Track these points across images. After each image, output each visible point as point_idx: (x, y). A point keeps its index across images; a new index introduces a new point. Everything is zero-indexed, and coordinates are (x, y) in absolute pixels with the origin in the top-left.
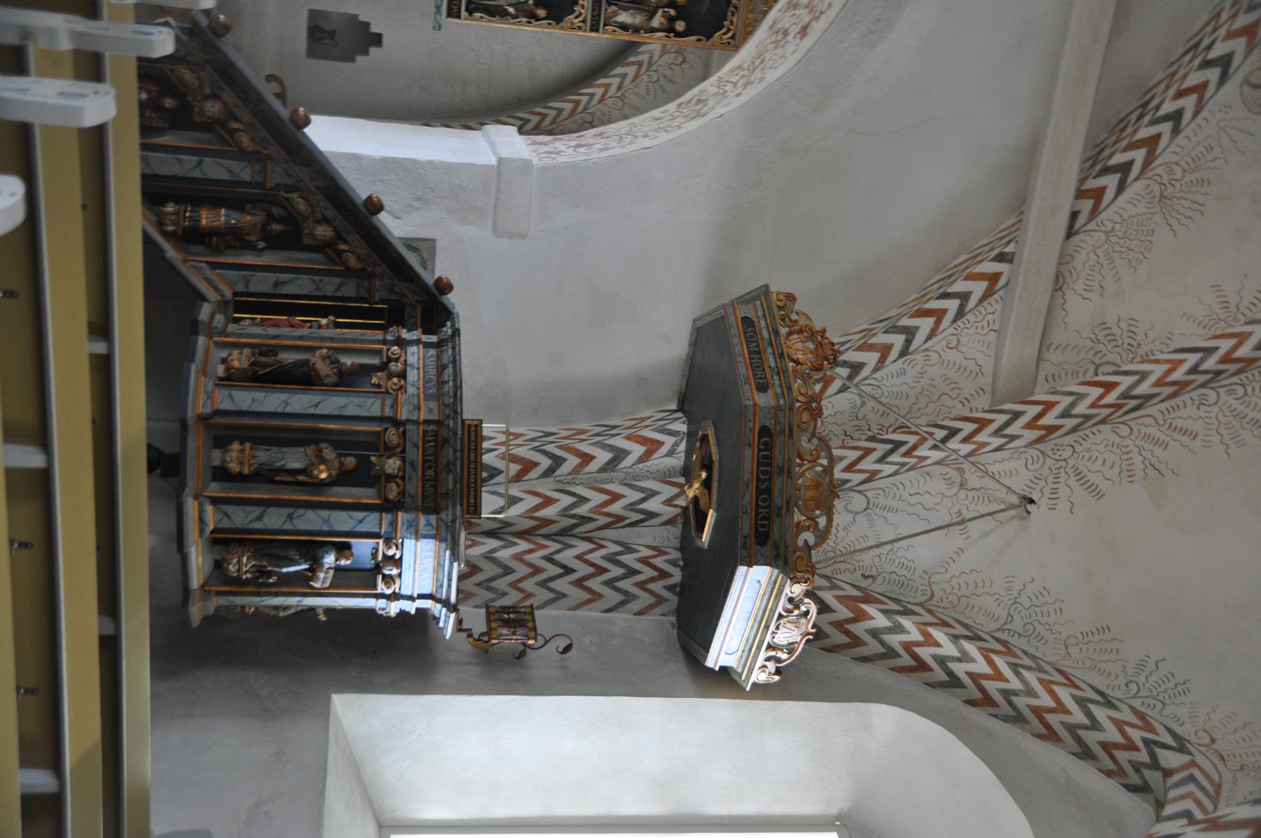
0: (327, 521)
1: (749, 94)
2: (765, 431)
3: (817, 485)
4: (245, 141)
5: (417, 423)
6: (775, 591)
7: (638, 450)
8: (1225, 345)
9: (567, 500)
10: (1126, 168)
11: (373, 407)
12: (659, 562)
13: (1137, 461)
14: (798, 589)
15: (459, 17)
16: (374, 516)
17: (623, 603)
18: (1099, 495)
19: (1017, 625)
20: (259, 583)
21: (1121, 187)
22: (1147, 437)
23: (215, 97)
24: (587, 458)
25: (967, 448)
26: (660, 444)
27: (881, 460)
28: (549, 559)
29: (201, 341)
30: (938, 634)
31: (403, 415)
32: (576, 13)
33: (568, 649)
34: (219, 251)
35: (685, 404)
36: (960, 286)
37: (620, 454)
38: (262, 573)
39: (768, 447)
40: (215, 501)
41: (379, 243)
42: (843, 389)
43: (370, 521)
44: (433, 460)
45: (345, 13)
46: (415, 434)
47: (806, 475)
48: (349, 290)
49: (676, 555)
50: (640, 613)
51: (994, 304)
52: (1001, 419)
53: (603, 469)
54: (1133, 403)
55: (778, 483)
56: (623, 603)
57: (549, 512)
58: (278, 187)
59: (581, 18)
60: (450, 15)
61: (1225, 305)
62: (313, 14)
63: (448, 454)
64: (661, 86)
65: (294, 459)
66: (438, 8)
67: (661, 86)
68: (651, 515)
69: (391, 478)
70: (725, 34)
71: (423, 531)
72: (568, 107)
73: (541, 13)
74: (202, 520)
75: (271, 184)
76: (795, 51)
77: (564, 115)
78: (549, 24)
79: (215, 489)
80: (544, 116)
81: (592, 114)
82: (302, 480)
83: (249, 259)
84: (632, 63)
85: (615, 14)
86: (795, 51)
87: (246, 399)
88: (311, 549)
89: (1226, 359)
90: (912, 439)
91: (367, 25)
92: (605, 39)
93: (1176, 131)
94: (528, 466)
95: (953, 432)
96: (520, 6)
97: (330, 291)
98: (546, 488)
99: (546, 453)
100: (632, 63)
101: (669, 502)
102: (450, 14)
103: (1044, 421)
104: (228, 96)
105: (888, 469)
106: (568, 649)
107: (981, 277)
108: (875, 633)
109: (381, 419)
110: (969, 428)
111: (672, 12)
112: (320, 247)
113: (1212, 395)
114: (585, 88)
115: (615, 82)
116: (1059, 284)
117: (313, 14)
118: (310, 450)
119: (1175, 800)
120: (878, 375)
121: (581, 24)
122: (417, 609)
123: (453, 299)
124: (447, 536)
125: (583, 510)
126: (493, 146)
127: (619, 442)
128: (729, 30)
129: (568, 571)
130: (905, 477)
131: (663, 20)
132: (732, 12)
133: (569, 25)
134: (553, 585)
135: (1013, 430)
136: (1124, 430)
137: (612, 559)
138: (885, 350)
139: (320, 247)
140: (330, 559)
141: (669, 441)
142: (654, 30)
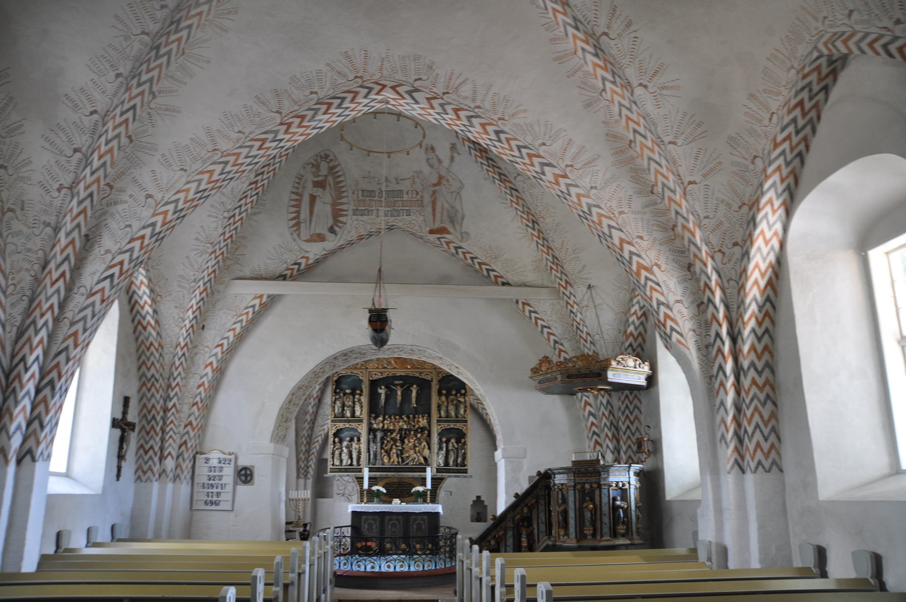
0: (605, 504)
1: (476, 382)
2: (568, 377)
3: (582, 360)
4: (501, 533)
5: (575, 480)
6: (615, 369)
7: (588, 408)
8: (535, 239)
9: (606, 429)
10: (488, 270)
11: (571, 493)
12: (623, 398)
13: (573, 256)
14: (614, 363)
16: (603, 490)
17: (638, 409)
18: (584, 266)
19: (626, 287)
20: (627, 523)
21: (493, 270)
22: (566, 254)
23: (489, 542)
24: (593, 424)
25: (576, 306)
26: (586, 401)
27: (582, 332)
28: (625, 433)
29: (558, 543)
30: (633, 311)
31: (572, 484)
33: (649, 427)
34: (534, 540)
35: (573, 394)
36: (527, 313)
37: (590, 413)
38: (623, 523)
39: (572, 375)
40: (602, 536)
41: (528, 493)
42: (562, 344)
43: (604, 491)
44: (586, 473)
46: (578, 480)
47: (580, 364)
48: (542, 502)
49: (620, 393)
50: (640, 402)
51: (531, 303)
52: (565, 298)
53: (595, 418)
54: (556, 260)
55: (583, 371)
56: (638, 409)
57: (610, 435)
58: (514, 524)
60: (466, 473)
61: (525, 236)
62: (472, 521)
63: (583, 470)
65: (588, 515)
66: (465, 477)
68: (608, 402)
69: (591, 486)
71: (606, 476)
73: (463, 441)
74: (607, 540)
75: (512, 525)
76: (462, 370)
79: (598, 537)
82: (594, 512)
83: (536, 532)
86: (462, 370)
87: (572, 530)
88: (615, 508)
89: (539, 238)
90: (575, 323)
92: (470, 417)
93: (476, 258)
94: (597, 442)
95: (571, 311)
97: (543, 507)
98: (603, 436)
99: (592, 437)
101: (603, 397)
102: (466, 472)
103: (564, 285)
104: (489, 538)
105: (585, 329)
106: (649, 427)
107: (523, 308)
108: (636, 329)
109: (575, 490)
110: (569, 307)
112: (530, 511)
113: (551, 239)
116: (525, 285)
117: (472, 521)
118: (585, 510)
119: (838, 50)
120: (557, 335)
122: (390, 503)
123: (542, 471)
124: (606, 468)
125: (608, 424)
126: (500, 460)
127: (586, 413)
129: (628, 427)
130: (587, 323)
134: (633, 431)
135: (568, 294)
136: (564, 261)
137: (623, 413)
138: (549, 333)
139: (530, 511)
140: (618, 503)
141: (585, 398)
142: (465, 401)
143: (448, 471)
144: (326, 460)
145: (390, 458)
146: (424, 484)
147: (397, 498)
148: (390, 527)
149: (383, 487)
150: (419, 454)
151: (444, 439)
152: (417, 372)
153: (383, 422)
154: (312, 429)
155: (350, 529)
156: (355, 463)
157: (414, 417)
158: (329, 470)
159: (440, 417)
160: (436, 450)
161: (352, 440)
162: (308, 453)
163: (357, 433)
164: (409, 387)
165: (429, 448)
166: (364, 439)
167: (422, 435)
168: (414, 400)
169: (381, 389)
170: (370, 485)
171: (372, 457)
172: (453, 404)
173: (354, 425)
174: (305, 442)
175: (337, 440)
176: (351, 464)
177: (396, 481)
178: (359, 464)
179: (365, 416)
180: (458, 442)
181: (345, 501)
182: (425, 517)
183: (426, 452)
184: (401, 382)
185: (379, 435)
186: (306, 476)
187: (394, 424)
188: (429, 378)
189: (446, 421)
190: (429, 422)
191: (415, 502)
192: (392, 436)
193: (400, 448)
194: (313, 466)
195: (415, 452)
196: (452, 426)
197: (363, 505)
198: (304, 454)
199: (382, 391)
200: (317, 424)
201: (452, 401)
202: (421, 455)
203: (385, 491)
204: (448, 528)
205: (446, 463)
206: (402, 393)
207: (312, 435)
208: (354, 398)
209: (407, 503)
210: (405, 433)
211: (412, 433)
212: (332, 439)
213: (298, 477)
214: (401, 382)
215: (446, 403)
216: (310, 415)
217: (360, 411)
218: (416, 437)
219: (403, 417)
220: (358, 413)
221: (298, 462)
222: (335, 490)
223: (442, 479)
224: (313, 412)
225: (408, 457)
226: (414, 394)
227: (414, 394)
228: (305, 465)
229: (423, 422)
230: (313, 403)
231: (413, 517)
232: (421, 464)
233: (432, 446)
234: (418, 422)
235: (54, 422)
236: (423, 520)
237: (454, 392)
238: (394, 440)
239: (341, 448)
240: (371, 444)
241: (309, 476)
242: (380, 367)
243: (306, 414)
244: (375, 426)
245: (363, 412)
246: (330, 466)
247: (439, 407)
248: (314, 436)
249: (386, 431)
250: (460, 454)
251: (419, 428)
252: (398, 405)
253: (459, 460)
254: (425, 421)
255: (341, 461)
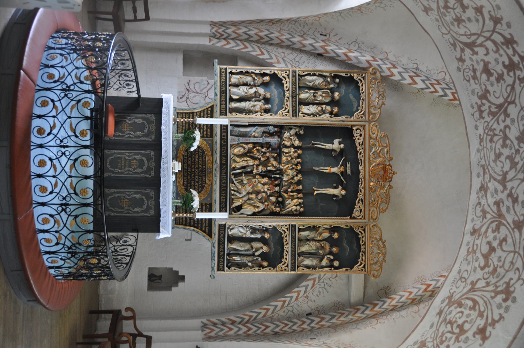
15: (223, 270)
32: (283, 262)
45: (166, 268)
59: (286, 265)
60: (219, 270)
62: (150, 269)
64: (326, 289)
66: (213, 268)
67: (326, 289)
70: (360, 266)
72: (280, 304)
73: (265, 264)
77: (278, 308)
78: (270, 269)
80: (268, 310)
81: (292, 307)
84: (311, 279)
85: (302, 261)
91: (177, 272)
96: (254, 262)
100: (311, 279)
111: (332, 257)
114: (288, 293)
115: (303, 289)
117: (150, 269)
121: (286, 268)
122: (175, 158)
128: (361, 264)
131: (327, 261)
132: (362, 254)
133: (280, 269)
142: (323, 267)
143: (221, 242)
144: (236, 64)
145: (238, 156)
146: (201, 210)
147: (183, 167)
148: (138, 157)
149: (199, 147)
150: (245, 198)
151: (267, 236)
152: (364, 195)
153: (293, 146)
154: (280, 45)
155: (135, 95)
156: (234, 105)
157: (298, 191)
158: (225, 67)
159: (300, 230)
160: (251, 224)
161: (267, 100)
162: (247, 40)
163: (275, 109)
164: (341, 183)
165: (254, 214)
166: (268, 118)
167: (273, 203)
168: (322, 191)
169: (340, 143)
170: (201, 127)
171: (243, 130)
172: (318, 248)
173: (288, 104)
174: (262, 34)
175: (267, 79)
176: (232, 100)
177: (208, 166)
178: (232, 110)
179: (300, 120)
180: (263, 256)
181: (179, 92)
182: (152, 213)
183: (248, 210)
184: (349, 172)
185: (274, 140)
186: (214, 36)
187: (288, 162)
188: (356, 213)
189: (293, 238)
190: (291, 214)
191: (177, 195)
192: (272, 160)
193: (255, 171)
194: (228, 47)
195: (248, 193)
196: (286, 247)
197: (172, 117)
198: (245, 33)
199: (336, 145)
200: (287, 52)
201: (322, 248)
202: (245, 202)
203: (192, 149)
204: (134, 253)
205: (232, 239)
206: (334, 174)
207: (271, 44)
208: (327, 104)
209: (176, 183)
210: (276, 179)
211: (277, 189)
212: (268, 72)
213: (213, 24)
214: (349, 172)
215: (319, 238)
216: (300, 42)
217: (309, 112)
218: (271, 195)
219: (300, 175)
220: (305, 109)
221: (234, 24)
222: (195, 79)
223: (210, 234)
224: (304, 46)
225: (241, 182)
226: (332, 191)
227: (332, 191)
228: (229, 35)
229: (292, 205)
230: (317, 45)
231: (152, 193)
232: (232, 203)
233: (258, 218)
234: (293, 198)
235: (202, 130)
236: (148, 209)
237: (335, 250)
238: (265, 164)
239: (255, 86)
240: (262, 129)
241: (215, 41)
242: (372, 142)
243: (302, 36)
244: (286, 135)
245: (307, 117)
246: (230, 68)
247: (314, 228)
248: (270, 48)
249: (278, 150)
250: (245, 260)
251: (284, 199)
252: (317, 169)
253: (237, 259)
254: (294, 208)
255: (236, 86)
